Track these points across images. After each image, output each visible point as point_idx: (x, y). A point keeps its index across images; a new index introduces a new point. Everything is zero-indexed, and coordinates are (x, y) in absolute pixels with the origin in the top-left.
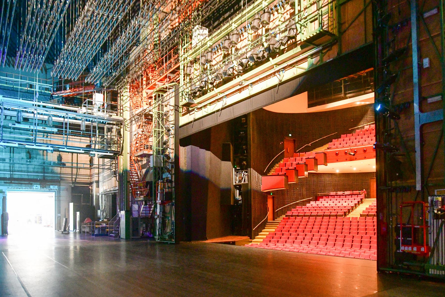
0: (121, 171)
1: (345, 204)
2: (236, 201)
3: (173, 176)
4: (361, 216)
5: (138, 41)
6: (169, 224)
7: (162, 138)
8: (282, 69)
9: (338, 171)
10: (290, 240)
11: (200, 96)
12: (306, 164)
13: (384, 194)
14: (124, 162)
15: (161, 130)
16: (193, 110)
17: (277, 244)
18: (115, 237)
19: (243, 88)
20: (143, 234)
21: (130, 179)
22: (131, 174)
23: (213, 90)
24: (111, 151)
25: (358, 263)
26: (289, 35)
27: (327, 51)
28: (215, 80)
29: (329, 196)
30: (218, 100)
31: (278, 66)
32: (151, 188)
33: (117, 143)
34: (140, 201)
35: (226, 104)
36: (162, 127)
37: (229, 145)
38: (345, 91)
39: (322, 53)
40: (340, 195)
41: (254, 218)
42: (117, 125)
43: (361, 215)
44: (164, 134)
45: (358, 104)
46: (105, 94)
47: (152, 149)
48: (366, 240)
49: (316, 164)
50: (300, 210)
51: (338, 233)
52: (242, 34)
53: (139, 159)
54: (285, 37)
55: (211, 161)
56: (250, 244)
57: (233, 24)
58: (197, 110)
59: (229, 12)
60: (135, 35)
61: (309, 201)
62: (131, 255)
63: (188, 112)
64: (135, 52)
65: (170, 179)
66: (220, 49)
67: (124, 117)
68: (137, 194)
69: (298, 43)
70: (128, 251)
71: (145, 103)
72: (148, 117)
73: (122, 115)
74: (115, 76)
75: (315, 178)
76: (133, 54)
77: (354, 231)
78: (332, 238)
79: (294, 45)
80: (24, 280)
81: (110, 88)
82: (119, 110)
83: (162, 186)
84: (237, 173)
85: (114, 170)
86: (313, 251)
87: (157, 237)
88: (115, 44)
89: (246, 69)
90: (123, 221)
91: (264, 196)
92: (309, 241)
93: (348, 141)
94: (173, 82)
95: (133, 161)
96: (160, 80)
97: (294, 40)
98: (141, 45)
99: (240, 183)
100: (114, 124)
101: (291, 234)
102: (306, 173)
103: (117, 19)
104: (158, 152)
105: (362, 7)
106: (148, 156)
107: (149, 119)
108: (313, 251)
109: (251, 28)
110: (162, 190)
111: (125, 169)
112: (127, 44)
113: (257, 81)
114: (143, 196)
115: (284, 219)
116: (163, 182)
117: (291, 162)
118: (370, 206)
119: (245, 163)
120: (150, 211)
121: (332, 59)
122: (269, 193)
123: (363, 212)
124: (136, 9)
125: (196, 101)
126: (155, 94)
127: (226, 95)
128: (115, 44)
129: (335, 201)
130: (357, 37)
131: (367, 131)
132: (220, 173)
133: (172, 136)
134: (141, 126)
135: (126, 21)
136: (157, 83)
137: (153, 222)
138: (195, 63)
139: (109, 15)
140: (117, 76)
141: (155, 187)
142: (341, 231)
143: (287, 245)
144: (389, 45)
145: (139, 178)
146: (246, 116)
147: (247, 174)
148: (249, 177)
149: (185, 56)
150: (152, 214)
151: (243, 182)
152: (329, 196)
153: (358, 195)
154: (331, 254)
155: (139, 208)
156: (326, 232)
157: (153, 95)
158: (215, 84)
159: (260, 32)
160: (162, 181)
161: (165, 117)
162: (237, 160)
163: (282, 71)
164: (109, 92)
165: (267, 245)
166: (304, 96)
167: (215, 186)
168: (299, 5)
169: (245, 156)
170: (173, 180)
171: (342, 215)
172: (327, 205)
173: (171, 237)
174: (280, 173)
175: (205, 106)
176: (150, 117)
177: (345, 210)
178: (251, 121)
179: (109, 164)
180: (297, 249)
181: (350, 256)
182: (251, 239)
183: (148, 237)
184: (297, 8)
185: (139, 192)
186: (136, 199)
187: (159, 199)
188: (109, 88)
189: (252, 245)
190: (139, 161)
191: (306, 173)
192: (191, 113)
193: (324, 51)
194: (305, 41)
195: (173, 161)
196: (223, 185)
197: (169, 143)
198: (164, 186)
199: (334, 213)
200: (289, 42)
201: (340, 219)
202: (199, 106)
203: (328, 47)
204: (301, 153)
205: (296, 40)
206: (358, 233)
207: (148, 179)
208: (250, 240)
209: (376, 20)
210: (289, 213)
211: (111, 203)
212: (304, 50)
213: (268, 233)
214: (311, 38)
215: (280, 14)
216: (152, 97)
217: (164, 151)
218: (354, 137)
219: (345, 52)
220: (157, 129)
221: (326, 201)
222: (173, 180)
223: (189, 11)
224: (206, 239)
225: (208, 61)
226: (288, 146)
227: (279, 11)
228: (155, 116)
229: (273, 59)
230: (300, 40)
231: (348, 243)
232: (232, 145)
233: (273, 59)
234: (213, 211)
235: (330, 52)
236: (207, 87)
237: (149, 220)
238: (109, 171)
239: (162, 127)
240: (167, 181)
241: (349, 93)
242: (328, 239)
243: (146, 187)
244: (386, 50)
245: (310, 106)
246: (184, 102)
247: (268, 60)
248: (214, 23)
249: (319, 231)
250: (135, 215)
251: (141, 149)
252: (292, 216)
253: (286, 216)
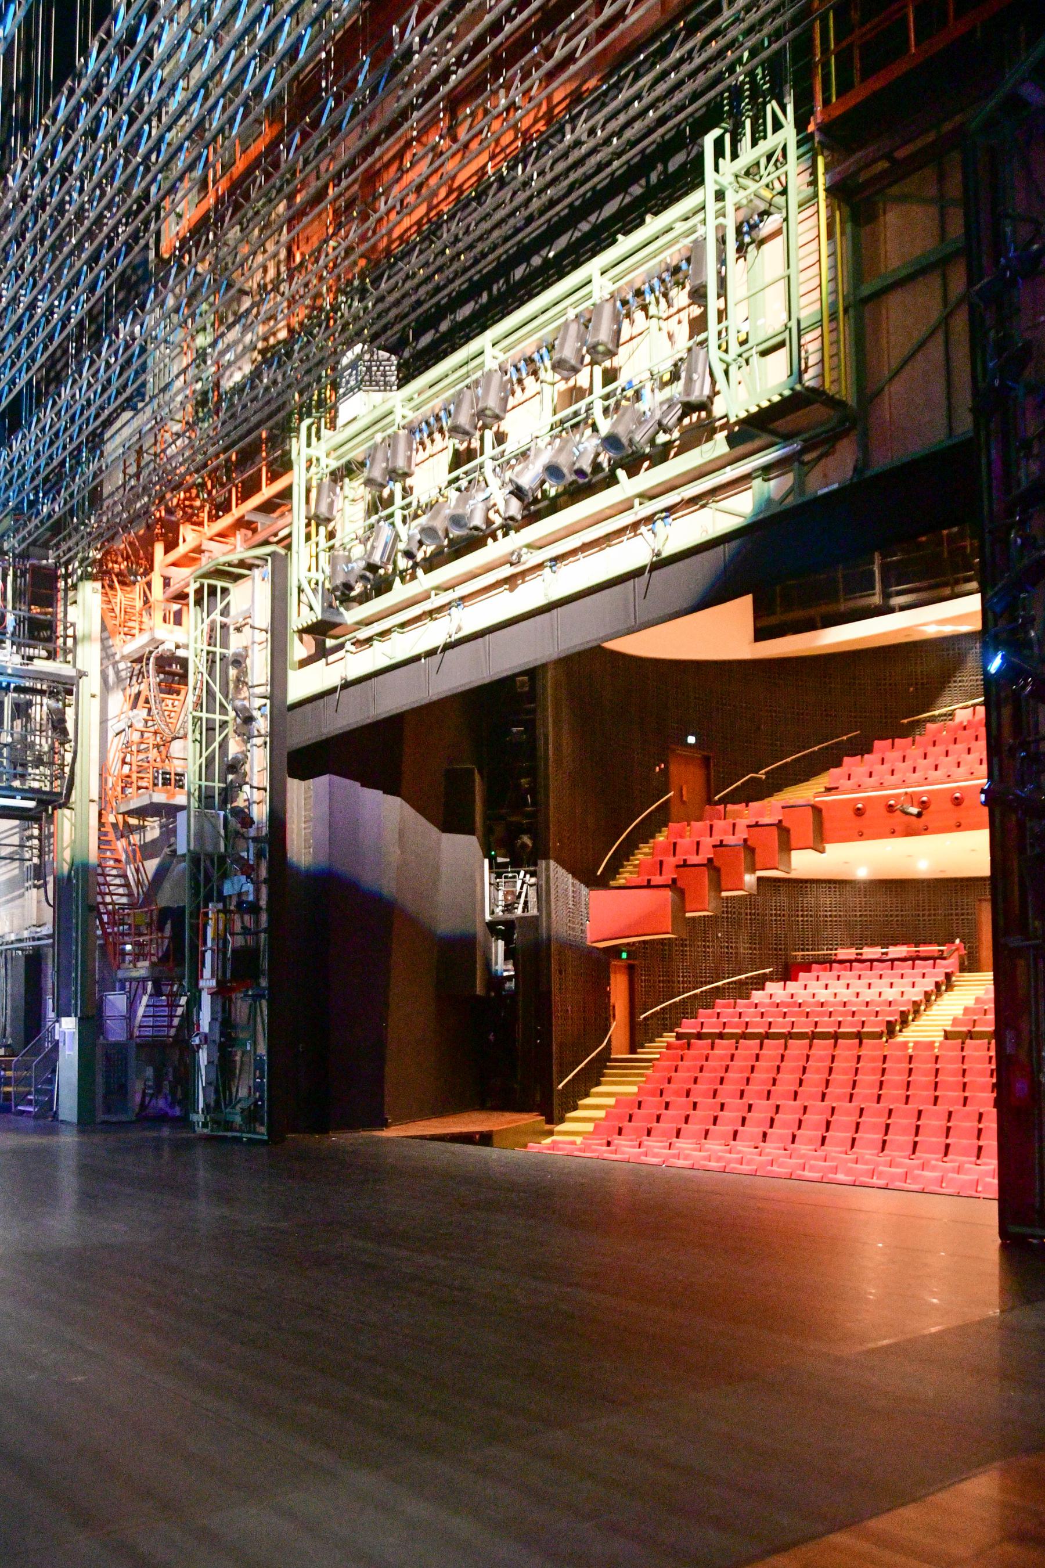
0: (66, 868)
1: (890, 994)
2: (496, 981)
3: (264, 890)
4: (946, 1038)
5: (140, 393)
6: (246, 1068)
7: (223, 745)
8: (662, 511)
9: (862, 873)
10: (693, 1127)
11: (364, 598)
12: (749, 848)
13: (1022, 963)
14: (75, 833)
15: (218, 717)
16: (341, 646)
17: (648, 1142)
18: (36, 1116)
19: (523, 574)
20: (143, 1106)
21: (99, 899)
22: (101, 879)
23: (414, 577)
24: (29, 794)
25: (940, 1208)
26: (686, 399)
27: (819, 458)
28: (421, 543)
29: (831, 962)
30: (430, 614)
31: (648, 503)
32: (177, 936)
33: (51, 763)
34: (138, 980)
35: (459, 629)
36: (222, 705)
37: (472, 771)
38: (885, 585)
39: (802, 463)
40: (872, 961)
41: (561, 1045)
42: (52, 694)
43: (947, 1035)
44: (232, 734)
45: (932, 631)
46: (10, 579)
47: (182, 787)
48: (964, 1124)
49: (786, 846)
50: (725, 1015)
51: (866, 1099)
52: (520, 381)
53: (133, 821)
54: (670, 403)
55: (401, 835)
56: (548, 1141)
57: (490, 349)
58: (353, 648)
59: (472, 304)
60: (130, 372)
61: (759, 983)
62: (99, 1186)
63: (321, 653)
64: (126, 432)
65: (251, 898)
66: (441, 430)
67: (79, 666)
68: (123, 953)
69: (718, 424)
70: (87, 1169)
71: (158, 616)
72: (172, 671)
73: (70, 657)
74: (49, 516)
75: (783, 899)
76: (118, 440)
77: (921, 1095)
78: (844, 1118)
79: (705, 431)
81: (28, 558)
82: (60, 641)
83: (221, 926)
84: (499, 876)
85: (36, 860)
86: (775, 1168)
87: (198, 1118)
88: (55, 403)
89: (535, 508)
90: (69, 1056)
91: (598, 963)
92: (760, 1130)
93: (900, 765)
94: (266, 543)
95: (108, 829)
96: (220, 535)
97: (703, 414)
98: (149, 410)
99: (508, 916)
100: (42, 692)
101: (695, 1104)
102: (750, 879)
103: (67, 317)
104: (206, 798)
105: (935, 314)
106: (169, 811)
107: (174, 674)
108: (775, 1168)
109: (554, 368)
110: (221, 939)
111: (78, 860)
112: (98, 403)
113: (573, 552)
114: (147, 964)
115: (669, 1046)
116: (225, 911)
117: (692, 838)
119: (526, 839)
120: (171, 1017)
121: (836, 486)
122: (615, 951)
123: (955, 1021)
124: (134, 278)
125: (351, 615)
126: (197, 585)
127: (463, 599)
128: (55, 403)
129: (855, 982)
130: (923, 412)
131: (965, 728)
132: (437, 869)
133: (259, 741)
134: (142, 699)
135: (96, 328)
136: (207, 545)
137: (181, 1059)
138: (347, 476)
139: (36, 299)
140: (56, 517)
141: (195, 928)
142: (876, 1091)
143: (681, 1144)
144: (1026, 445)
145: (130, 895)
146: (533, 673)
147: (533, 880)
148: (543, 895)
149: (312, 453)
150: (179, 1028)
151: (519, 911)
152: (831, 962)
153: (935, 959)
154: (841, 1177)
155: (132, 1005)
156: (824, 1095)
157: (191, 590)
158: (420, 555)
159: (582, 379)
160: (220, 906)
161: (233, 672)
162: (500, 830)
163: (663, 519)
164: (23, 575)
165: (609, 1144)
166: (742, 608)
167: (420, 930)
168: (719, 296)
169: (528, 816)
170: (263, 903)
171: (880, 1035)
172: (823, 995)
173: (252, 1116)
174: (657, 880)
175: (383, 634)
176: (176, 668)
177: (890, 1014)
178: (550, 691)
179: (15, 840)
180: (719, 1159)
181: (906, 1186)
182: (550, 1121)
183: (161, 1118)
184: (714, 303)
185: (128, 947)
186: (120, 974)
187: (207, 972)
188: (24, 556)
189: (554, 1145)
190: (131, 829)
191: (750, 879)
192: (331, 658)
193: (807, 458)
194: (741, 422)
195: (265, 831)
196: (446, 924)
197: (247, 767)
198: (228, 929)
199: (852, 1025)
200: (686, 421)
201: (874, 1048)
202: (363, 634)
203: (822, 443)
204: (730, 807)
205: (709, 413)
206: (936, 1098)
207: (165, 898)
208: (548, 1127)
209: (985, 364)
210: (688, 1027)
212: (741, 449)
213: (612, 1101)
214: (762, 412)
215: (654, 320)
216: (186, 596)
217: (228, 793)
219: (882, 461)
220: (204, 715)
221: (822, 982)
222: (263, 903)
223: (329, 290)
224: (384, 1124)
225: (395, 475)
226: (685, 779)
227: (652, 309)
228: (197, 666)
229: (630, 476)
230: (726, 416)
231: (900, 1138)
232: (480, 772)
233: (630, 476)
234: (409, 1015)
235: (830, 462)
236: (390, 568)
237: (170, 1052)
238: (17, 864)
239: (222, 705)
240: (240, 904)
241: (900, 593)
242: (828, 1123)
243: (161, 929)
244: (1018, 466)
245: (761, 634)
246: (308, 618)
247: (611, 481)
248: (416, 338)
249: (796, 1093)
250: (116, 1032)
251: (141, 784)
252: (699, 1036)
253: (679, 1037)
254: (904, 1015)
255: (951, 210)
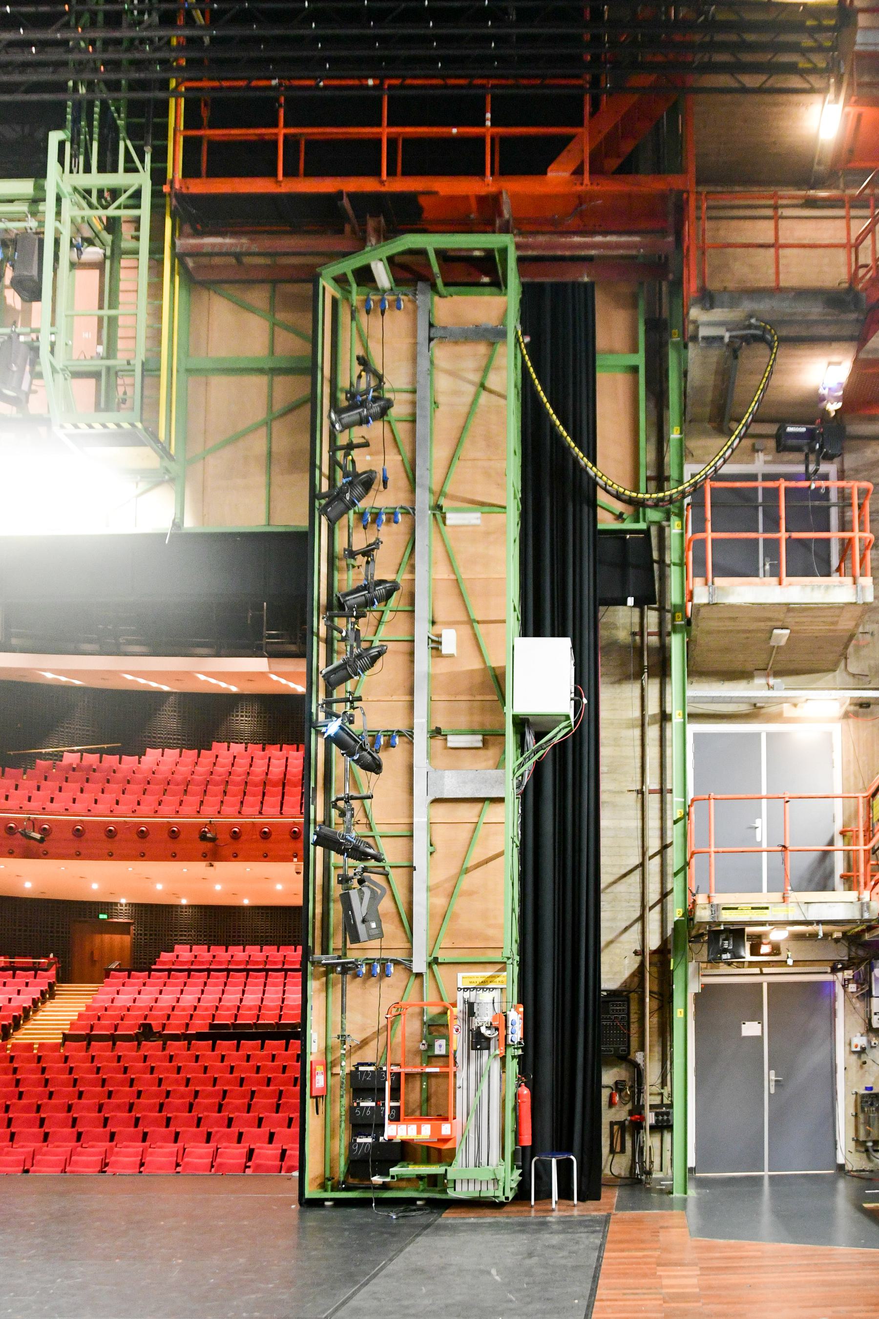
51: (207, 1108)
80: (817, 98)
118: (88, 1008)
131: (74, 769)
211: (474, 178)
218: (34, 783)
254: (16, 1019)
255: (779, 213)
